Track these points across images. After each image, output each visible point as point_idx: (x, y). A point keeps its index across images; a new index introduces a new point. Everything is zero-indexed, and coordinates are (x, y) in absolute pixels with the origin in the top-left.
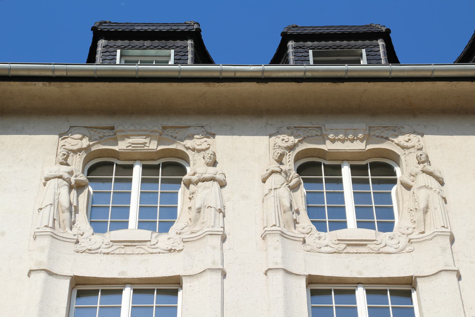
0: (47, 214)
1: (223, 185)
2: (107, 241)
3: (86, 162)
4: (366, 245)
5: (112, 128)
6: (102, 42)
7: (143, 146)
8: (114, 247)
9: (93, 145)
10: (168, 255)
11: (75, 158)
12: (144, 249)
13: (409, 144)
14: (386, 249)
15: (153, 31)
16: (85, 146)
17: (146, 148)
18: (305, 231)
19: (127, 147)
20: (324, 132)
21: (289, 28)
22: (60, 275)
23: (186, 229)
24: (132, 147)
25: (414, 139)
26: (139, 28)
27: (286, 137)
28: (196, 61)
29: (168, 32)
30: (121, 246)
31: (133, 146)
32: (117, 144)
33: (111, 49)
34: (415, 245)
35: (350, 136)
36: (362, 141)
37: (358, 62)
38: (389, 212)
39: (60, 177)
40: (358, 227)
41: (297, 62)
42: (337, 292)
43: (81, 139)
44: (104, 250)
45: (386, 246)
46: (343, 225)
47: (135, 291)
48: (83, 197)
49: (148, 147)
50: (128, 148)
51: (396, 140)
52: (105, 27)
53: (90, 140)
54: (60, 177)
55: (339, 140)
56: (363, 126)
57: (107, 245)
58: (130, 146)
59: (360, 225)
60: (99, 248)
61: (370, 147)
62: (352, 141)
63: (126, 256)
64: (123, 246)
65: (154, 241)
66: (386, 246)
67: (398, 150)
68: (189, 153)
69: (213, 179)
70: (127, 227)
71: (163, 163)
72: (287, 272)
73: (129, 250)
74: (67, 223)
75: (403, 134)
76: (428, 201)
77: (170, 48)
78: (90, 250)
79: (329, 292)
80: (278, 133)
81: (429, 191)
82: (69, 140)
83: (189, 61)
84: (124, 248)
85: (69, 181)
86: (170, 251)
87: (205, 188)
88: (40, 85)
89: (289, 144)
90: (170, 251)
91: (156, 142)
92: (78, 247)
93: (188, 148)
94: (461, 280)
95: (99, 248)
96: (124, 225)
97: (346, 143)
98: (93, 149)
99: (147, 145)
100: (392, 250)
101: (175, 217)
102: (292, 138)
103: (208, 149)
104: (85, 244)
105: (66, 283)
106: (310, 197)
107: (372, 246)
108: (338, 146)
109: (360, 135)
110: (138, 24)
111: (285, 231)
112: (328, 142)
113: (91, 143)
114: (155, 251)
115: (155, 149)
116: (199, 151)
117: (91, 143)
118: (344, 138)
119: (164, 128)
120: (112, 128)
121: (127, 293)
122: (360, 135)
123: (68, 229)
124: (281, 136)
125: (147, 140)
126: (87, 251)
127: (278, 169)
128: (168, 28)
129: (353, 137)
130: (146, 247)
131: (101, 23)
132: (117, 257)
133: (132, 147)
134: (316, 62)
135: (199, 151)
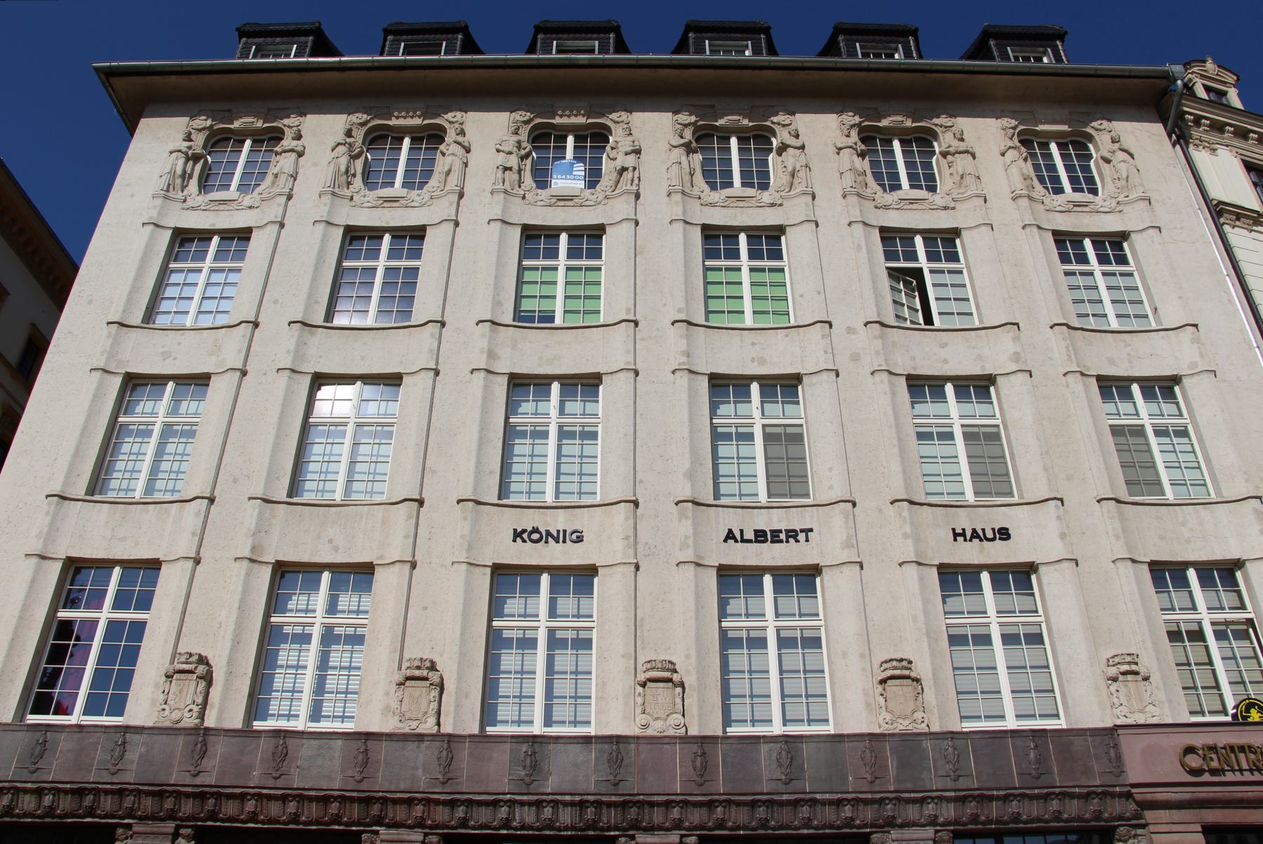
0: (165, 180)
1: (300, 154)
2: (206, 200)
3: (694, 133)
5: (713, 106)
6: (540, 36)
9: (863, 122)
10: (248, 211)
13: (619, 120)
14: (412, 204)
15: (282, 30)
16: (208, 125)
18: (355, 190)
21: (391, 25)
23: (267, 190)
25: (624, 116)
26: (271, 28)
27: (360, 115)
28: (617, 51)
29: (294, 30)
32: (880, 122)
33: (549, 41)
34: (434, 200)
35: (575, 112)
36: (583, 116)
37: (439, 53)
38: (765, 175)
39: (180, 151)
40: (742, 186)
41: (696, 53)
42: (546, 236)
43: (206, 120)
46: (731, 185)
47: (393, 237)
48: (529, 162)
51: (611, 117)
52: (248, 28)
53: (213, 120)
54: (180, 151)
55: (565, 115)
59: (744, 185)
61: (426, 122)
62: (412, 117)
63: (219, 212)
65: (759, 197)
67: (446, 125)
68: (776, 128)
69: (292, 150)
70: (393, 187)
71: (591, 134)
72: (686, 222)
73: (221, 207)
74: (179, 187)
75: (451, 111)
76: (451, 166)
77: (747, 40)
79: (540, 237)
81: (454, 158)
82: (680, 115)
83: (611, 51)
85: (186, 154)
86: (250, 207)
87: (285, 158)
88: (173, 78)
90: (250, 207)
91: (262, 121)
92: (185, 205)
93: (285, 126)
96: (392, 184)
97: (407, 119)
98: (215, 128)
100: (416, 204)
101: (600, 176)
102: (365, 116)
103: (789, 125)
104: (190, 203)
105: (518, 230)
106: (705, 162)
107: (403, 202)
108: (401, 122)
109: (418, 113)
110: (271, 25)
111: (337, 190)
112: (557, 117)
114: (759, 205)
116: (784, 126)
119: (753, 107)
120: (230, 111)
121: (387, 238)
122: (582, 112)
123: (180, 192)
127: (343, 142)
128: (294, 27)
130: (234, 205)
131: (244, 25)
132: (212, 213)
134: (559, 52)
135: (784, 126)
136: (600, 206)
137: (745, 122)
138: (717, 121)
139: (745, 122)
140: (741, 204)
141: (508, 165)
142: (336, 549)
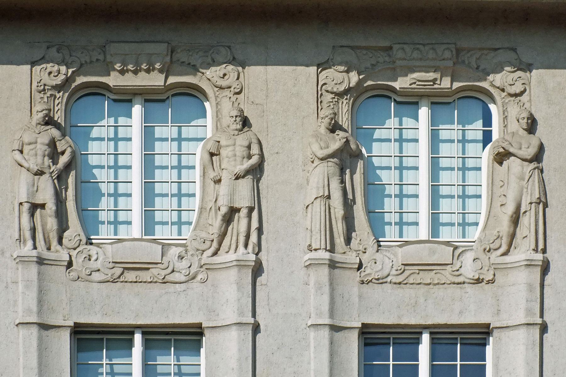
4: (148, 269)
7: (432, 83)
8: (407, 273)
11: (340, 103)
12: (441, 274)
17: (436, 86)
19: (410, 85)
20: (109, 58)
22: (511, 326)
24: (417, 85)
30: (414, 271)
31: (418, 83)
43: (347, 72)
44: (394, 277)
45: (173, 271)
49: (440, 85)
50: (413, 86)
56: (162, 48)
57: (397, 270)
58: (415, 83)
60: (388, 275)
64: (417, 271)
66: (173, 271)
78: (378, 279)
80: (43, 60)
84: (418, 274)
89: (59, 80)
94: (260, 333)
95: (388, 275)
99: (438, 82)
113: (361, 77)
115: (448, 88)
117: (361, 77)
118: (122, 68)
122: (157, 66)
124: (49, 65)
125: (437, 75)
126: (374, 281)
129: (122, 67)
133: (417, 85)
136: (195, 284)
137: (446, 83)
138: (396, 80)
139: (446, 83)
140: (427, 277)
141: (39, 201)
142: (249, 333)
